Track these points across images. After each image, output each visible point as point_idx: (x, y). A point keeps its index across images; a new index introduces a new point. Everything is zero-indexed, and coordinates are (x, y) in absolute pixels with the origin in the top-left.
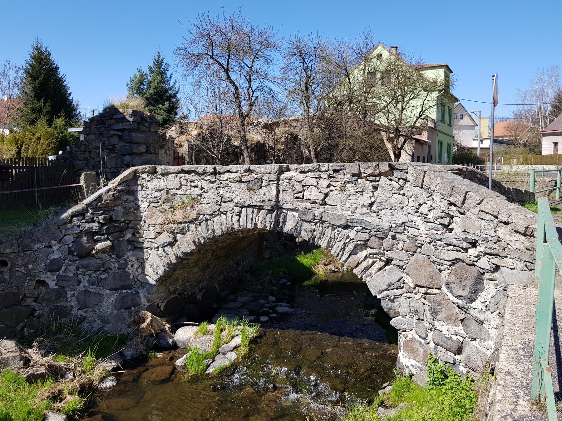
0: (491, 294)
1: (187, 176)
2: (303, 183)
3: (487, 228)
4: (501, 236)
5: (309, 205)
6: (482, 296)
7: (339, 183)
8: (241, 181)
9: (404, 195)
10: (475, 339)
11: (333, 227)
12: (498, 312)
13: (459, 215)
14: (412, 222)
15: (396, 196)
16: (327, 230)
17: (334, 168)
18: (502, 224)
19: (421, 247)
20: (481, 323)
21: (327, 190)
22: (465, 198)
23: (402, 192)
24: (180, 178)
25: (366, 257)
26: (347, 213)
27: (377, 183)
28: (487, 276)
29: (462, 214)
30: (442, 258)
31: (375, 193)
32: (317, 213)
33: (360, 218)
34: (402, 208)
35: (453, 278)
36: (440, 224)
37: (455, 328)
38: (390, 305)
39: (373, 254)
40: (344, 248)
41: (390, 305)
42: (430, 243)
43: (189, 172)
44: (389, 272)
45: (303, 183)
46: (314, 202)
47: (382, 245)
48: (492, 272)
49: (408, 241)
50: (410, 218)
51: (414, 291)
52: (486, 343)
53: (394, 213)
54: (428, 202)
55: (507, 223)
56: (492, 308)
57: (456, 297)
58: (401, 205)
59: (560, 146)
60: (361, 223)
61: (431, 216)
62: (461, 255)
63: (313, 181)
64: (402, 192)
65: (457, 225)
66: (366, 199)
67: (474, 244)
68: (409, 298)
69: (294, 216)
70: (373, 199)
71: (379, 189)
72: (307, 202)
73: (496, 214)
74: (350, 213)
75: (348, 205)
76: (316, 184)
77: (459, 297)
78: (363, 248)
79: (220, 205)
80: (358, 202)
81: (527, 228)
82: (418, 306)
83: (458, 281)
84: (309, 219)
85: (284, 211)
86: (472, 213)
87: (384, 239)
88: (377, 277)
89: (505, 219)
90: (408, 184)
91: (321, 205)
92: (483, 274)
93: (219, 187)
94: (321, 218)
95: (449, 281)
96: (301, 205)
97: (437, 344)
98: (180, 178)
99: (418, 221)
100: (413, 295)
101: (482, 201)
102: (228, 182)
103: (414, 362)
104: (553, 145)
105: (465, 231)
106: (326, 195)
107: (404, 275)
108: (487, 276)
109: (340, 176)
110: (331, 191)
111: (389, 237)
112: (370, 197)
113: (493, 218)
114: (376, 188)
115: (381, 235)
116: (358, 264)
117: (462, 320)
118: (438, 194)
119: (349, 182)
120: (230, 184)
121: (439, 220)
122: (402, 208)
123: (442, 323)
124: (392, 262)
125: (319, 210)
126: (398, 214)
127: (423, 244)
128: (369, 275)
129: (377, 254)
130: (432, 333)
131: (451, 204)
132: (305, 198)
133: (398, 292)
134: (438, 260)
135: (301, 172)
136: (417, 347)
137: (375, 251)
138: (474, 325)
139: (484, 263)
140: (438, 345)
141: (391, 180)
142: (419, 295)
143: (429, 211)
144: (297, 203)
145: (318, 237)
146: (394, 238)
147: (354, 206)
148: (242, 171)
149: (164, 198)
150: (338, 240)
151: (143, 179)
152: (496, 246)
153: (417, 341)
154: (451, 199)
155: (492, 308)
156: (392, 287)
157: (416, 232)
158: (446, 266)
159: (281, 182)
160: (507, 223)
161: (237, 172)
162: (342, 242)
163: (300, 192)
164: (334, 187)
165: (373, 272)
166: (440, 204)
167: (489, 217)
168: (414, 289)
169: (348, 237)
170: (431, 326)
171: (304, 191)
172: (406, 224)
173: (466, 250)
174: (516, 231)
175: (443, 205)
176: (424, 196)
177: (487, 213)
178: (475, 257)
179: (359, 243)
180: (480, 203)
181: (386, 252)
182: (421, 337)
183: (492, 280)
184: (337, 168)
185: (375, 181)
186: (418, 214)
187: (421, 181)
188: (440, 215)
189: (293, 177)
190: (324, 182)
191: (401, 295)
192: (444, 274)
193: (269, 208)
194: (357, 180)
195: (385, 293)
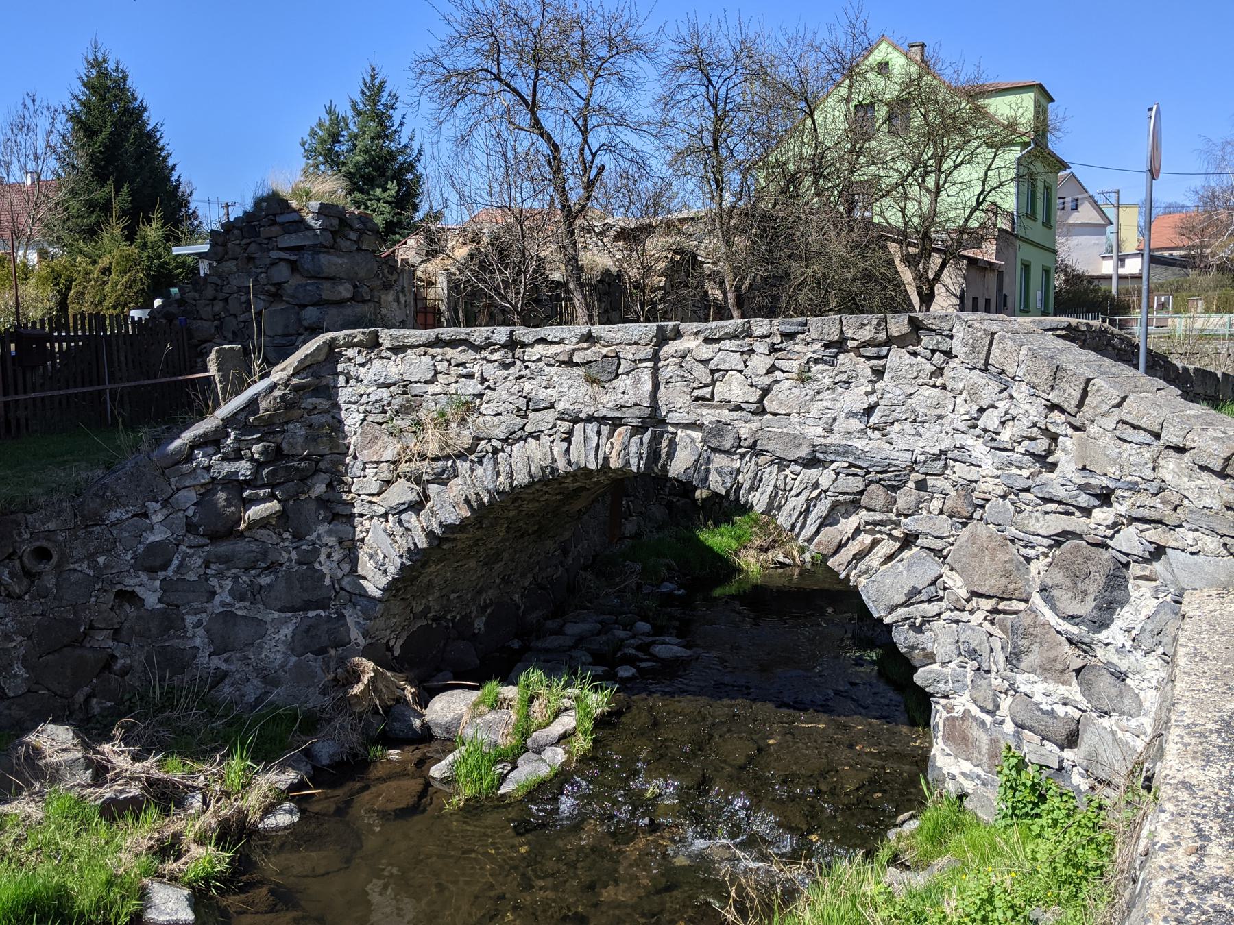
1: (450, 353)
2: (712, 365)
5: (726, 415)
6: (1125, 617)
7: (795, 364)
8: (570, 363)
9: (944, 387)
12: (1160, 650)
13: (1070, 431)
14: (962, 448)
15: (927, 391)
16: (768, 470)
17: (782, 328)
18: (1171, 452)
20: (1121, 677)
21: (766, 381)
22: (1085, 394)
23: (939, 382)
24: (433, 357)
25: (857, 531)
26: (814, 432)
27: (882, 362)
28: (1135, 570)
29: (1076, 429)
30: (1032, 530)
31: (878, 385)
32: (744, 433)
34: (941, 417)
35: (1057, 577)
36: (1027, 453)
37: (1063, 690)
38: (913, 638)
39: (874, 523)
41: (913, 638)
42: (1004, 497)
43: (453, 344)
44: (911, 565)
45: (712, 365)
46: (739, 408)
48: (1146, 561)
49: (953, 494)
50: (959, 440)
52: (1133, 723)
55: (1181, 450)
56: (1147, 642)
57: (1064, 618)
58: (938, 412)
60: (844, 454)
61: (1006, 436)
62: (1076, 523)
63: (735, 360)
64: (939, 382)
66: (856, 398)
67: (1105, 498)
68: (957, 622)
70: (872, 399)
71: (886, 377)
72: (721, 408)
73: (1156, 429)
75: (815, 412)
76: (741, 367)
77: (1071, 618)
78: (851, 509)
79: (525, 417)
83: (1068, 582)
84: (728, 446)
85: (671, 429)
86: (1101, 429)
89: (1176, 441)
90: (954, 363)
91: (754, 413)
93: (522, 377)
94: (755, 443)
95: (1049, 582)
96: (709, 415)
97: (1020, 726)
98: (433, 357)
99: (978, 448)
100: (964, 616)
101: (1124, 399)
102: (541, 364)
103: (967, 767)
105: (1084, 468)
106: (766, 391)
109: (798, 348)
110: (777, 381)
111: (911, 484)
114: (879, 373)
115: (891, 479)
116: (841, 546)
117: (1078, 672)
119: (817, 361)
120: (547, 369)
121: (1025, 443)
122: (941, 417)
124: (919, 542)
125: (748, 425)
126: (930, 430)
127: (988, 500)
128: (866, 572)
129: (883, 523)
131: (1052, 407)
132: (717, 399)
133: (933, 608)
135: (707, 341)
136: (976, 732)
137: (878, 516)
138: (1105, 683)
139: (1130, 540)
140: (1022, 727)
141: (915, 354)
142: (980, 615)
143: (1003, 423)
144: (699, 411)
145: (746, 486)
146: (921, 486)
147: (830, 414)
148: (574, 340)
150: (794, 492)
151: (350, 360)
152: (1156, 502)
153: (975, 719)
156: (917, 598)
157: (973, 474)
158: (1041, 549)
160: (1181, 450)
161: (561, 341)
162: (802, 498)
163: (706, 386)
165: (875, 564)
166: (1027, 407)
167: (1141, 436)
169: (816, 485)
171: (714, 382)
172: (950, 454)
173: (1087, 512)
175: (1034, 411)
176: (989, 389)
177: (1135, 427)
178: (1108, 527)
179: (841, 498)
180: (1119, 405)
182: (983, 709)
185: (879, 358)
186: (977, 431)
187: (982, 356)
188: (1028, 433)
189: (690, 351)
190: (760, 362)
191: (939, 615)
192: (1035, 567)
193: (636, 422)
194: (835, 356)
195: (902, 611)
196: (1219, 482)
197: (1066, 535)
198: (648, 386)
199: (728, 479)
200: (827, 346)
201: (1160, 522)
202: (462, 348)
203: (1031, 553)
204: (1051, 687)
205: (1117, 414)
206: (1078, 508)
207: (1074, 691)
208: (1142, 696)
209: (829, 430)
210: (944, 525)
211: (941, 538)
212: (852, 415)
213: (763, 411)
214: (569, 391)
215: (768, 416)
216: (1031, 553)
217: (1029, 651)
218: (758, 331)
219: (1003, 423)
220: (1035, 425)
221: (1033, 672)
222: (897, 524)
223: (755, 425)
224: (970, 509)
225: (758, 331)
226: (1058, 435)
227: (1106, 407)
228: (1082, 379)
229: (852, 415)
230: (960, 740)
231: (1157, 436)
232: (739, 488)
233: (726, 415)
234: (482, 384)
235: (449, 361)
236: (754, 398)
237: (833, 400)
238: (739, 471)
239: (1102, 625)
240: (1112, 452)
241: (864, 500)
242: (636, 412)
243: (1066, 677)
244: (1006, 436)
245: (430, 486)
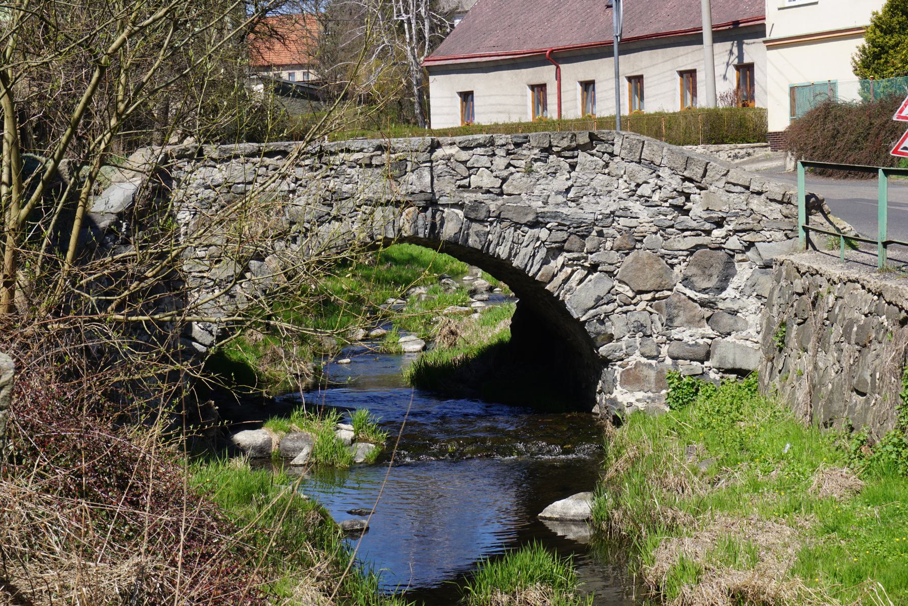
0: (746, 277)
1: (268, 161)
2: (469, 164)
3: (738, 200)
4: (754, 208)
5: (480, 196)
6: (735, 282)
7: (523, 162)
8: (369, 165)
9: (609, 174)
10: (729, 334)
11: (517, 226)
12: (755, 294)
13: (698, 191)
14: (626, 209)
15: (600, 177)
16: (508, 231)
17: (515, 140)
18: (755, 195)
19: (641, 241)
20: (734, 313)
21: (505, 173)
22: (706, 171)
23: (607, 171)
24: (254, 164)
25: (563, 266)
26: (537, 204)
27: (575, 160)
28: (738, 257)
29: (701, 189)
30: (676, 248)
31: (573, 174)
32: (493, 207)
33: (555, 210)
34: (610, 192)
35: (694, 270)
36: (672, 206)
37: (701, 331)
38: (600, 328)
39: (574, 259)
40: (534, 256)
41: (600, 328)
42: (656, 233)
43: (270, 154)
44: (596, 283)
45: (469, 164)
46: (488, 192)
47: (584, 246)
48: (743, 252)
49: (619, 237)
50: (623, 204)
51: (633, 302)
52: (744, 333)
53: (599, 200)
54: (651, 181)
55: (759, 193)
56: (748, 291)
57: (699, 292)
58: (608, 189)
59: (477, 101)
60: (555, 217)
61: (656, 197)
62: (703, 239)
63: (485, 161)
64: (607, 171)
65: (697, 208)
66: (561, 182)
67: (719, 224)
68: (626, 313)
69: (457, 215)
70: (570, 183)
71: (577, 169)
72: (476, 192)
73: (747, 184)
74: (540, 204)
75: (536, 192)
76: (489, 165)
77: (704, 291)
78: (557, 253)
79: (331, 205)
80: (550, 187)
81: (784, 195)
82: (644, 318)
83: (700, 272)
84: (482, 217)
85: (441, 208)
86: (717, 188)
87: (587, 236)
88: (580, 291)
89: (758, 189)
90: (617, 159)
91: (498, 195)
92: (733, 256)
93: (328, 176)
94: (500, 214)
95: (689, 274)
96: (468, 198)
97: (675, 358)
98: (254, 164)
99: (636, 207)
100: (632, 307)
101: (728, 171)
102: (344, 167)
103: (640, 395)
104: (459, 99)
105: (708, 209)
106: (504, 180)
107: (616, 283)
108: (738, 257)
109: (525, 152)
110: (512, 174)
111: (594, 233)
112: (567, 179)
113: (743, 190)
114: (573, 167)
115: (582, 231)
116: (554, 276)
117: (708, 319)
118: (667, 169)
119: (536, 160)
120: (349, 171)
121: (670, 201)
122: (610, 192)
123: (682, 329)
124: (599, 268)
125: (495, 203)
126: (604, 200)
127: (644, 237)
128: (569, 291)
129: (578, 259)
130: (667, 346)
131: (685, 179)
132: (473, 186)
133: (610, 307)
134: (669, 252)
135: (465, 148)
136: (646, 372)
137: (575, 255)
138: (727, 319)
139: (734, 243)
140: (677, 358)
141: (592, 155)
142: (643, 305)
143: (653, 191)
144: (461, 195)
145: (495, 242)
146: (600, 234)
147: (546, 193)
148: (372, 149)
149: (222, 200)
150: (524, 244)
151: (180, 168)
152: (750, 220)
153: (645, 365)
154: (686, 174)
155: (748, 291)
156: (601, 302)
157: (634, 223)
158: (681, 258)
159: (434, 164)
160: (759, 193)
161: (361, 150)
162: (530, 248)
163: (465, 178)
164: (515, 167)
165: (574, 285)
166: (670, 180)
167: (739, 189)
168: (632, 298)
169: (538, 239)
170: (665, 338)
171: (470, 176)
172: (617, 213)
173: (708, 233)
174: (771, 200)
175: (676, 182)
176: (643, 173)
177: (735, 185)
178: (723, 238)
179: (554, 245)
180: (725, 175)
181: (590, 256)
182: (648, 357)
183: (743, 261)
184: (520, 141)
185: (573, 157)
186: (635, 198)
187: (638, 154)
188: (670, 195)
189: (453, 155)
190: (500, 162)
191: (613, 311)
192: (677, 269)
193: (422, 204)
194: (548, 157)
195: (592, 312)
196: (780, 206)
197: (698, 247)
198: (428, 179)
199: (483, 239)
200: (542, 151)
201: (752, 230)
202: (279, 157)
203: (675, 261)
204: (694, 330)
205: (724, 179)
206: (704, 231)
207: (708, 330)
208: (747, 319)
209: (546, 203)
210: (615, 256)
211: (612, 264)
212: (558, 193)
213: (501, 194)
214: (370, 185)
215: (505, 196)
216: (675, 261)
217: (678, 316)
218: (499, 142)
219: (653, 191)
220: (675, 190)
221: (682, 325)
222: (586, 259)
223: (500, 202)
224: (632, 243)
225: (499, 142)
226: (690, 194)
227: (718, 177)
228: (704, 163)
229: (558, 193)
230: (632, 379)
231: (747, 188)
232: (490, 242)
233: (480, 196)
234: (295, 183)
235: (267, 167)
236: (498, 185)
237: (547, 184)
238: (489, 233)
239: (723, 289)
240: (724, 198)
241: (566, 246)
242: (422, 196)
243: (701, 324)
244: (656, 197)
245: (252, 262)
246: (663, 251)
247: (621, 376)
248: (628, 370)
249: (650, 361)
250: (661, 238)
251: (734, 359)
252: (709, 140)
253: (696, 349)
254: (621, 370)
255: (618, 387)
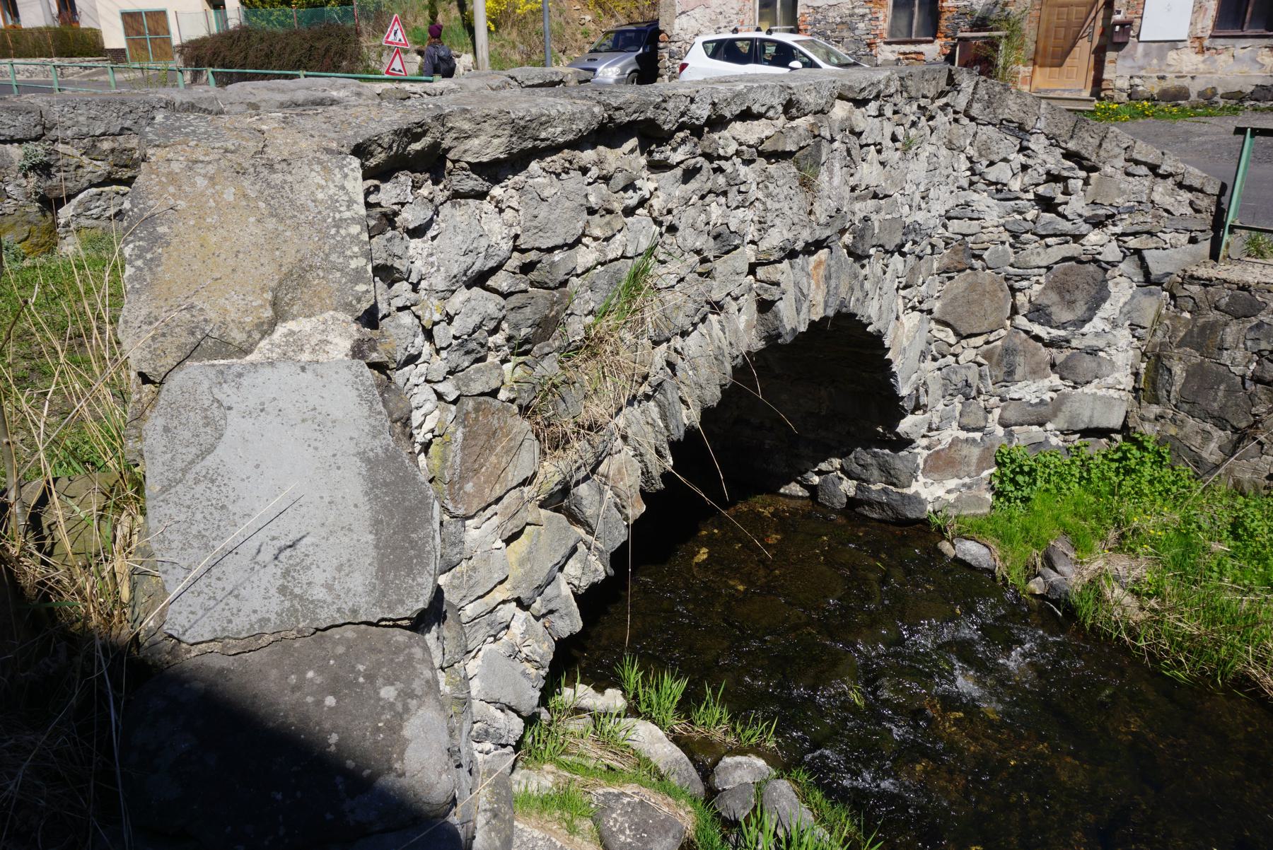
0: (1123, 300)
6: (1108, 309)
20: (1093, 352)
30: (1034, 264)
37: (1046, 382)
99: (981, 200)
103: (952, 483)
105: (1093, 203)
118: (1043, 137)
123: (1024, 383)
154: (1072, 145)
166: (1045, 157)
202: (633, 142)
246: (1011, 270)
247: (926, 461)
248: (937, 452)
249: (971, 435)
250: (1011, 250)
251: (1091, 417)
252: (60, 54)
253: (1043, 409)
254: (926, 453)
255: (920, 478)
